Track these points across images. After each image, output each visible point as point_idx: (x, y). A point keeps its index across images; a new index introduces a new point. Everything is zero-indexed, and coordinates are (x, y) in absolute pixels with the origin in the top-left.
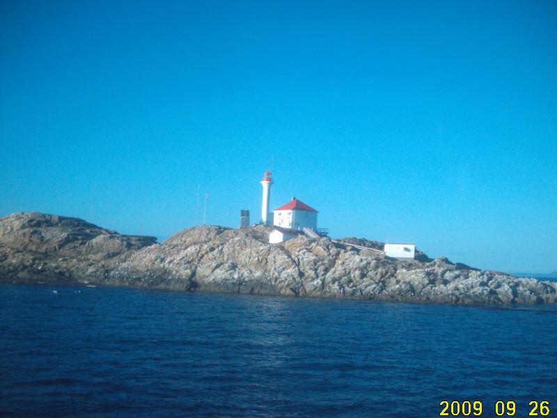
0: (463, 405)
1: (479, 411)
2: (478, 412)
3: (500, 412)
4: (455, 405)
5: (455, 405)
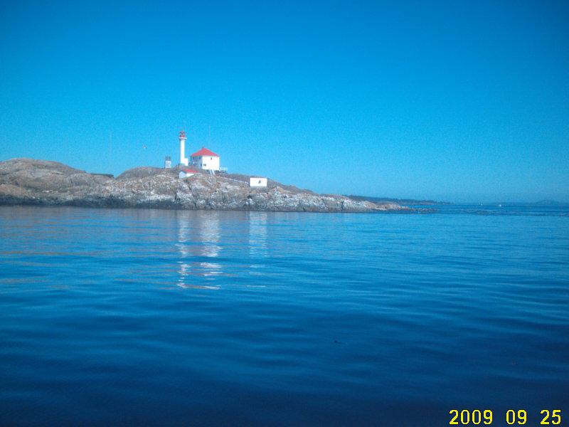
0: (473, 414)
1: (523, 420)
2: (522, 421)
3: (511, 421)
4: (465, 413)
5: (465, 413)
